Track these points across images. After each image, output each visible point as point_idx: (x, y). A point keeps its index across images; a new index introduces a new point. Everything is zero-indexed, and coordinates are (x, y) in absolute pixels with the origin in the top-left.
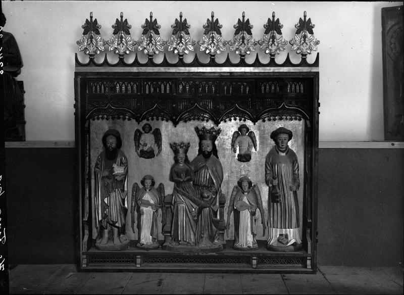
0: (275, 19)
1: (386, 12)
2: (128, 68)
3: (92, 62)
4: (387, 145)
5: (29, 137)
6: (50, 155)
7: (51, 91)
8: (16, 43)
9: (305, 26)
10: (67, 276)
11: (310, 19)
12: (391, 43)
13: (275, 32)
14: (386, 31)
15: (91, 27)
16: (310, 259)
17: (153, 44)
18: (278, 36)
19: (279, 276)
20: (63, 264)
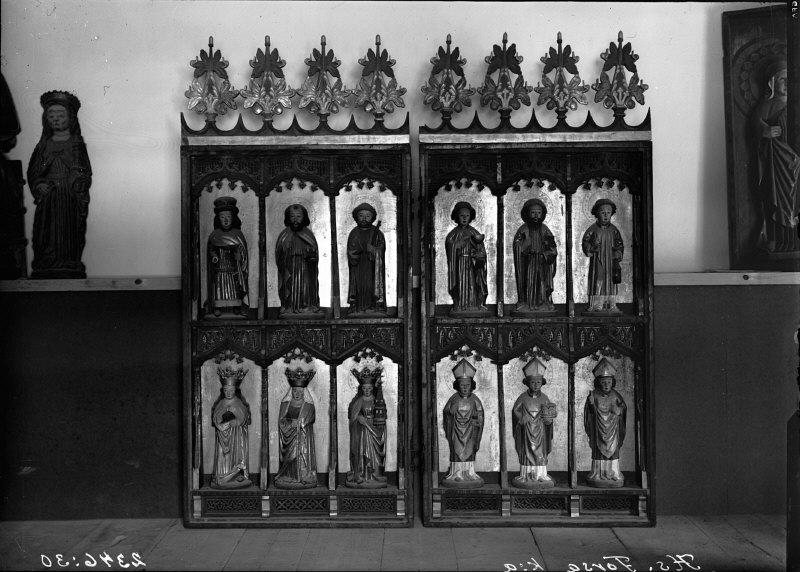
1: (732, 25)
2: (337, 137)
3: (211, 128)
4: (734, 278)
5: (90, 272)
6: (134, 305)
7: (135, 182)
8: (11, 99)
9: (620, 56)
10: (114, 542)
13: (565, 70)
15: (210, 64)
16: (643, 500)
17: (271, 97)
18: (569, 77)
19: (525, 530)
20: (104, 518)
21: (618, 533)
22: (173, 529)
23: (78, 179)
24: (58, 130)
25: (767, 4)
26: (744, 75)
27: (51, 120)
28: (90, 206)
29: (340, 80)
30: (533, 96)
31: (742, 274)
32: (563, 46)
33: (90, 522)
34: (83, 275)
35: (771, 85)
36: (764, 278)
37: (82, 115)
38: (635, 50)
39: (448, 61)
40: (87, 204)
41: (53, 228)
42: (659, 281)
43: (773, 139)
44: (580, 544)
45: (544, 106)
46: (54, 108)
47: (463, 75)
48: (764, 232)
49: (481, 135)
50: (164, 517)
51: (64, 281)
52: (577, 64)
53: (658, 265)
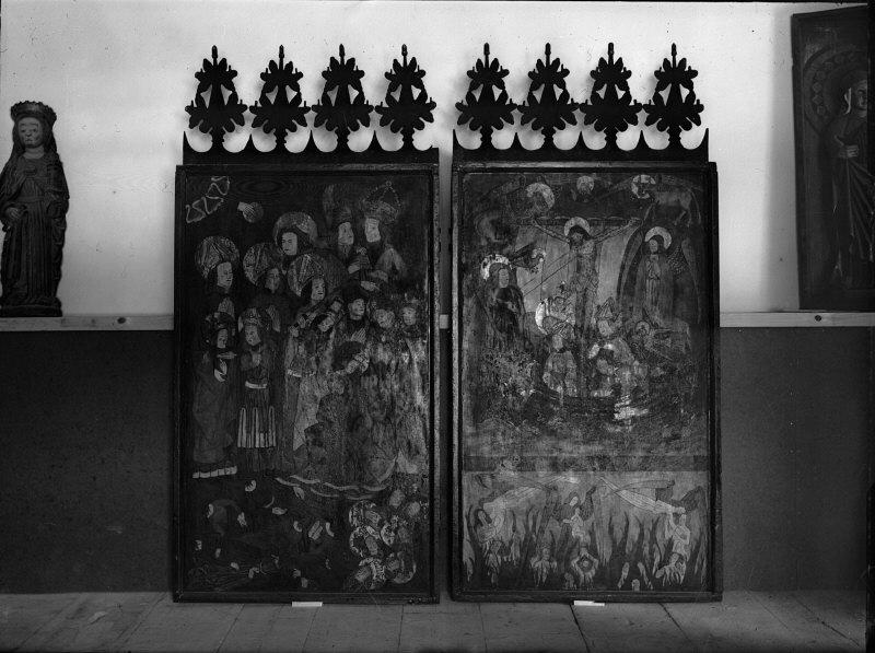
0: (615, 60)
1: (802, 28)
4: (805, 319)
5: (65, 309)
6: (114, 345)
11: (620, 59)
12: (813, 94)
14: (802, 66)
15: (216, 74)
21: (669, 610)
22: (160, 604)
23: (54, 203)
24: (31, 146)
25: (845, 5)
26: (816, 87)
27: (23, 134)
28: (67, 233)
29: (299, 95)
30: (310, 116)
31: (815, 314)
32: (552, 60)
33: (64, 595)
34: (59, 314)
35: (848, 99)
36: (839, 319)
37: (58, 130)
38: (422, 64)
39: (487, 74)
40: (64, 231)
41: (24, 258)
42: (723, 324)
43: (849, 160)
44: (627, 622)
45: (529, 126)
46: (25, 121)
47: (361, 88)
48: (838, 266)
49: (625, 154)
50: (151, 590)
51: (38, 319)
52: (361, 80)
53: (725, 303)
